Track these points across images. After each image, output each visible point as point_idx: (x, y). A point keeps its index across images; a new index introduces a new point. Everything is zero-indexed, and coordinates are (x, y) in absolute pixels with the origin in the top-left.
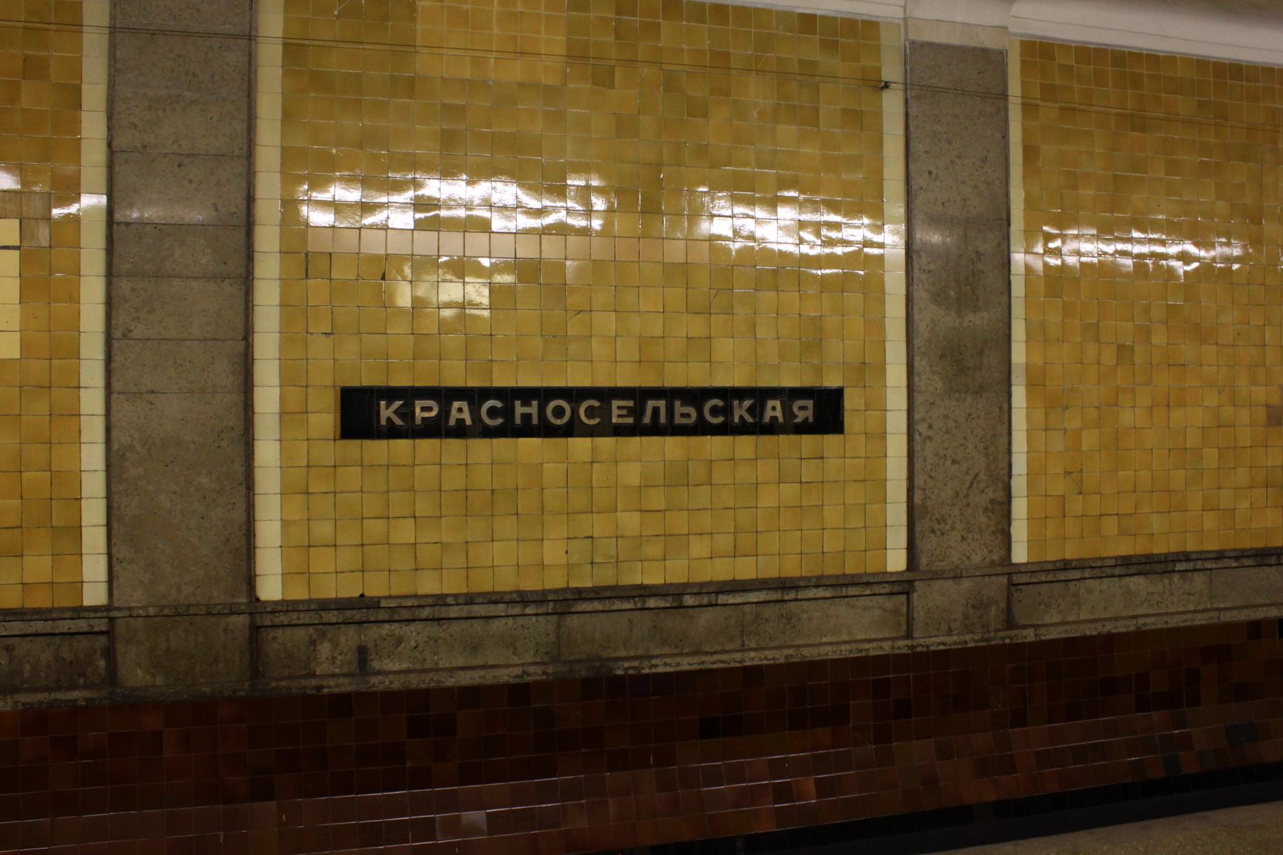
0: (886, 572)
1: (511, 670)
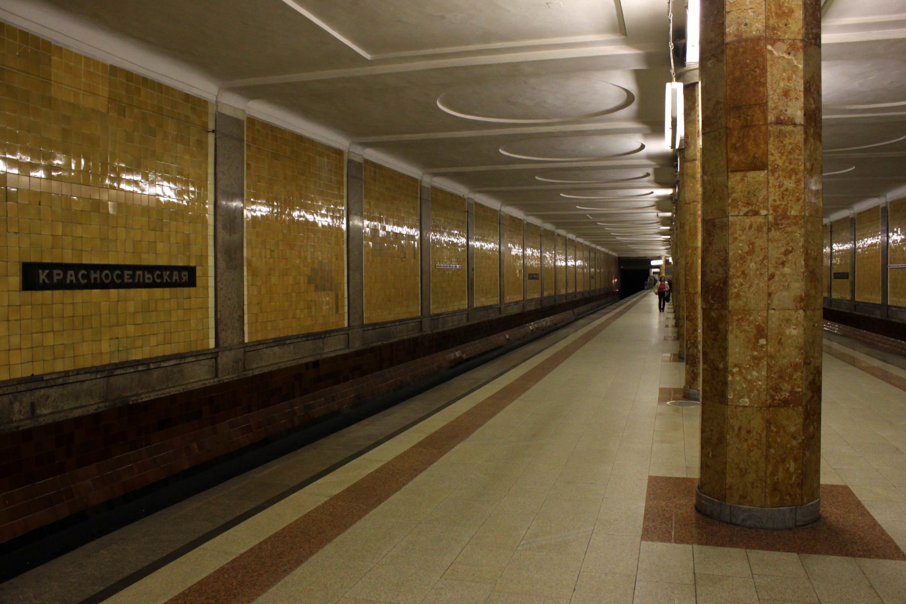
1: (93, 407)
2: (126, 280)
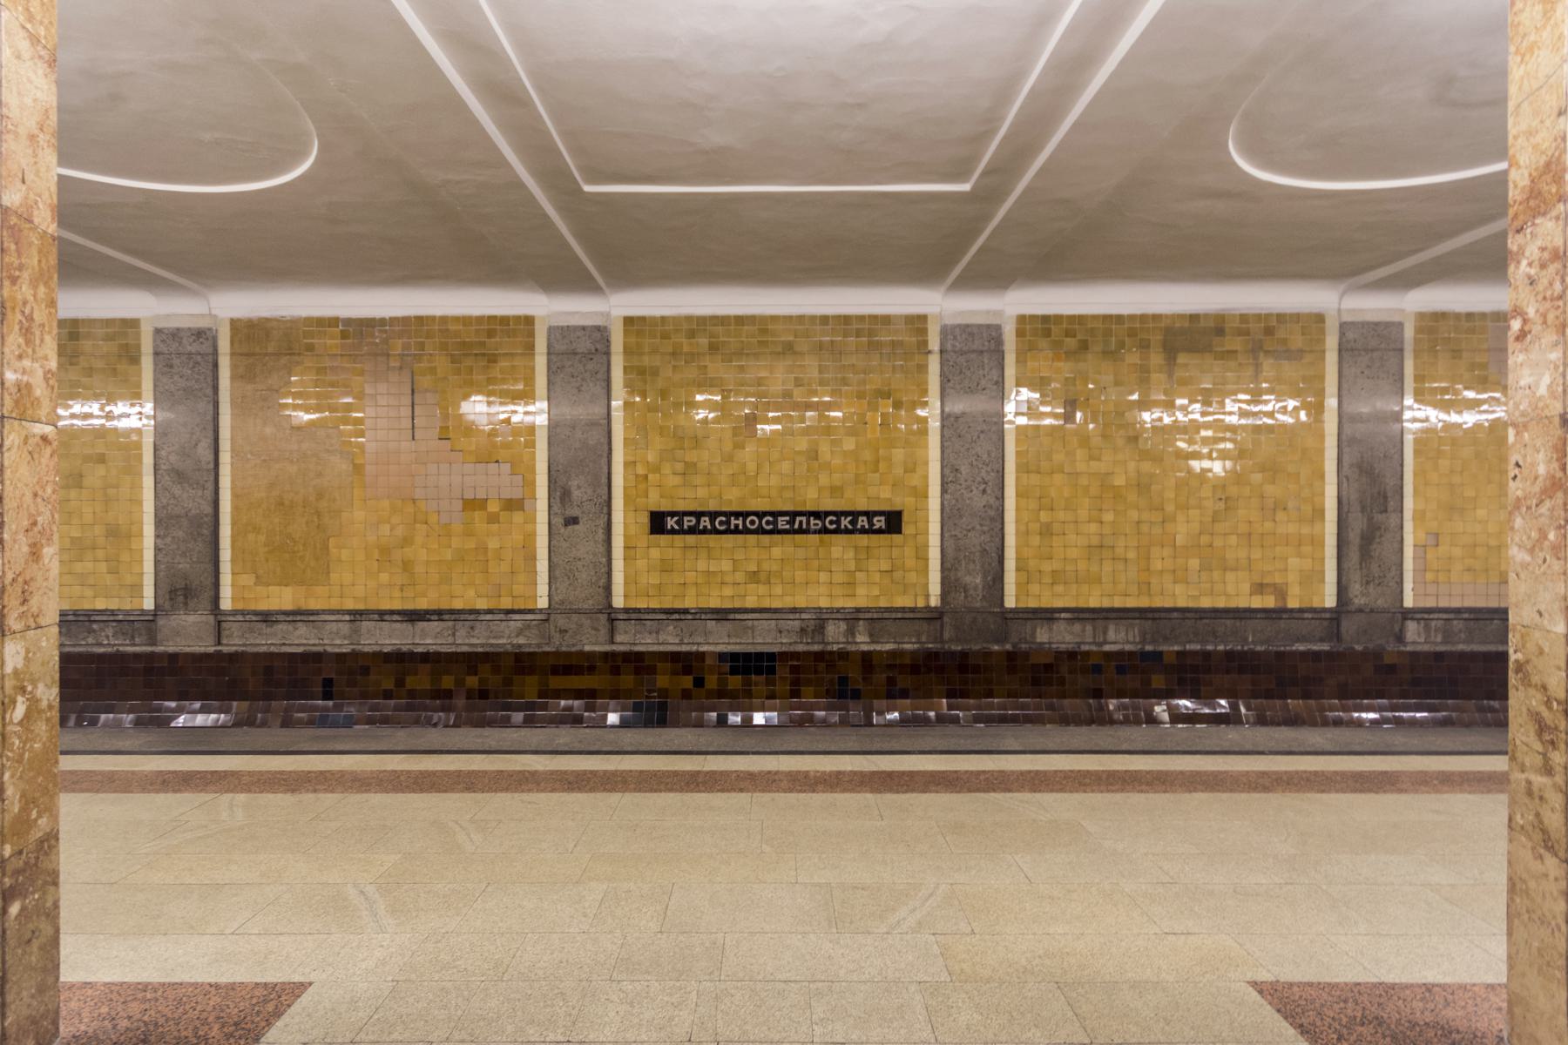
2: (780, 527)
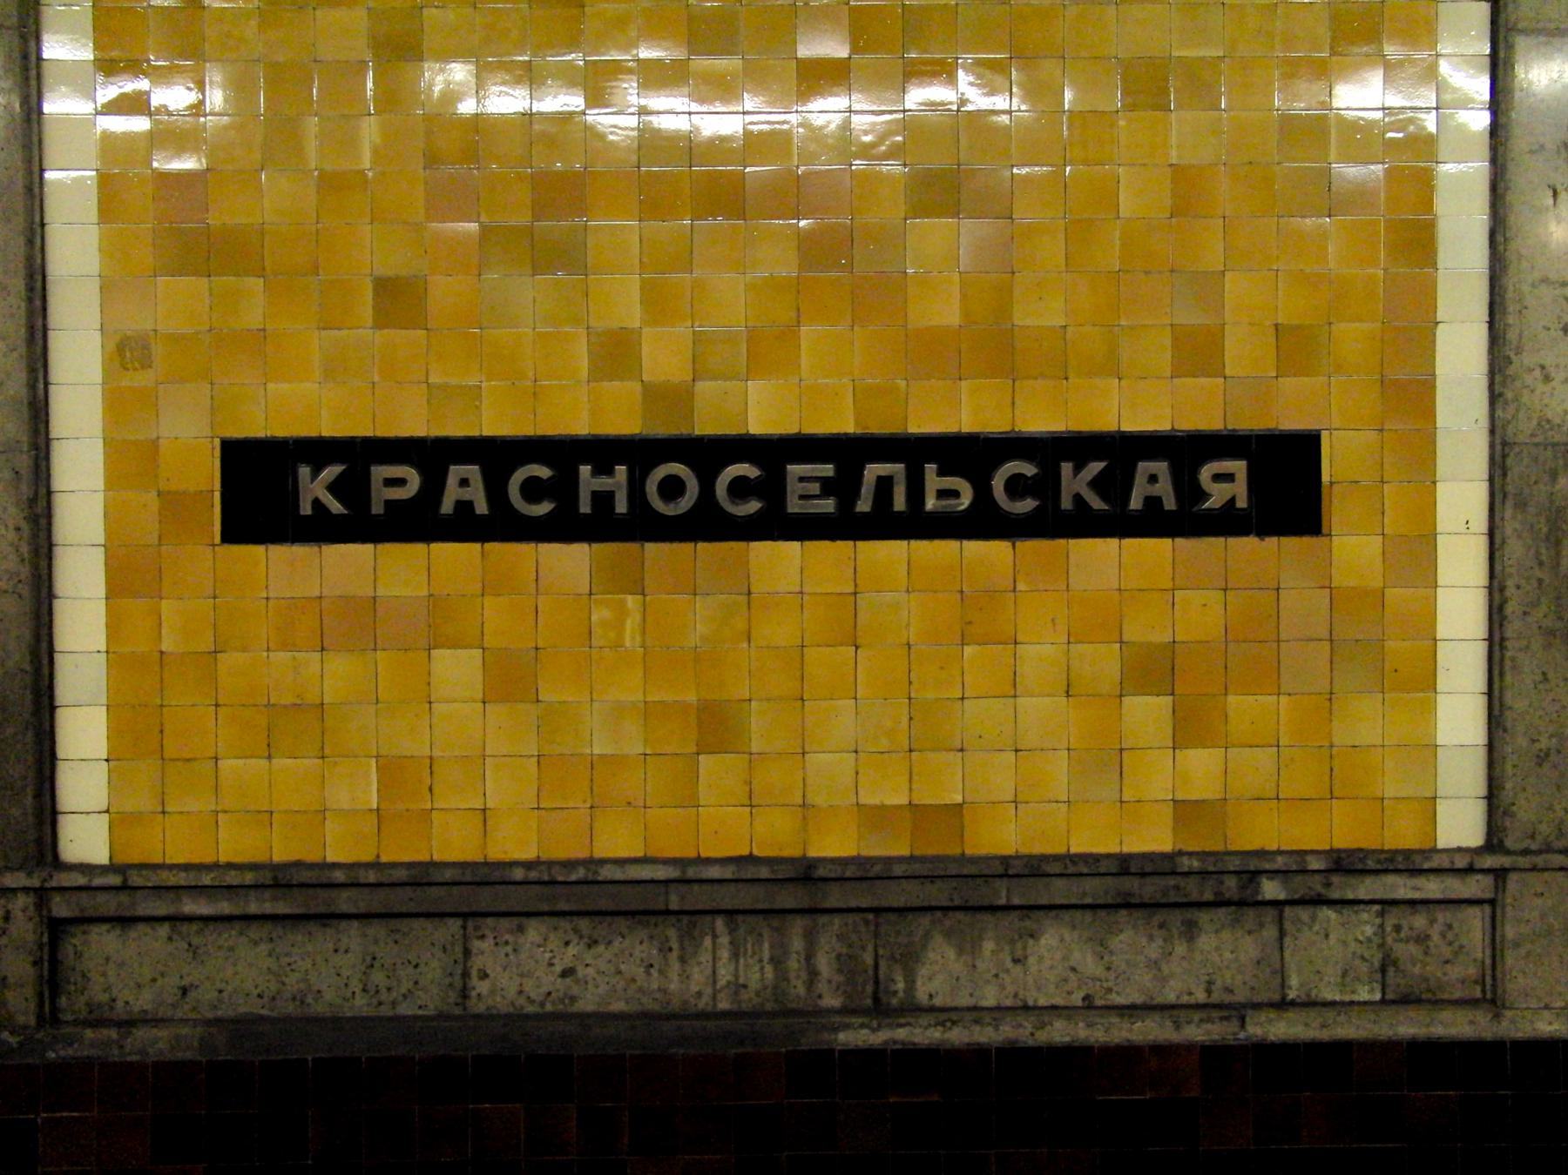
0: (1435, 850)
2: (794, 506)
